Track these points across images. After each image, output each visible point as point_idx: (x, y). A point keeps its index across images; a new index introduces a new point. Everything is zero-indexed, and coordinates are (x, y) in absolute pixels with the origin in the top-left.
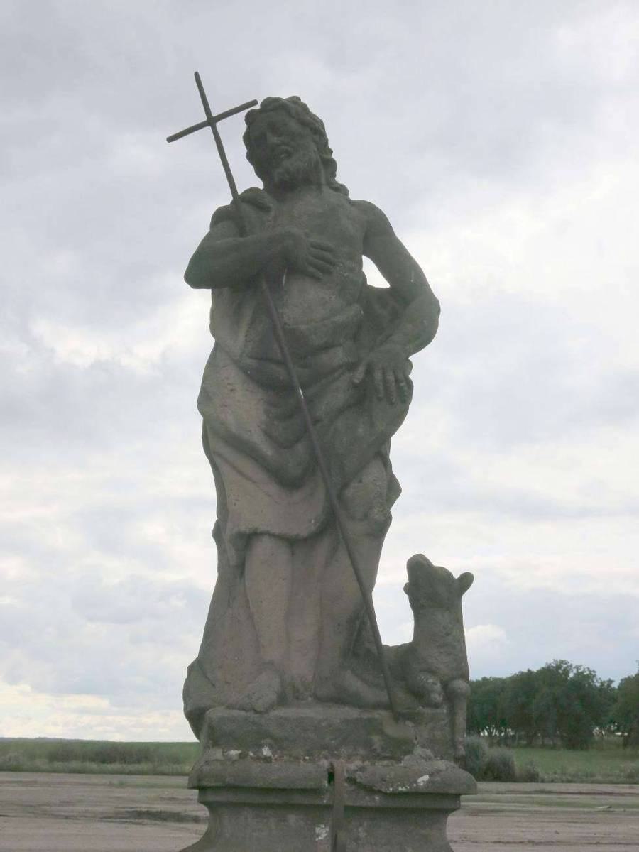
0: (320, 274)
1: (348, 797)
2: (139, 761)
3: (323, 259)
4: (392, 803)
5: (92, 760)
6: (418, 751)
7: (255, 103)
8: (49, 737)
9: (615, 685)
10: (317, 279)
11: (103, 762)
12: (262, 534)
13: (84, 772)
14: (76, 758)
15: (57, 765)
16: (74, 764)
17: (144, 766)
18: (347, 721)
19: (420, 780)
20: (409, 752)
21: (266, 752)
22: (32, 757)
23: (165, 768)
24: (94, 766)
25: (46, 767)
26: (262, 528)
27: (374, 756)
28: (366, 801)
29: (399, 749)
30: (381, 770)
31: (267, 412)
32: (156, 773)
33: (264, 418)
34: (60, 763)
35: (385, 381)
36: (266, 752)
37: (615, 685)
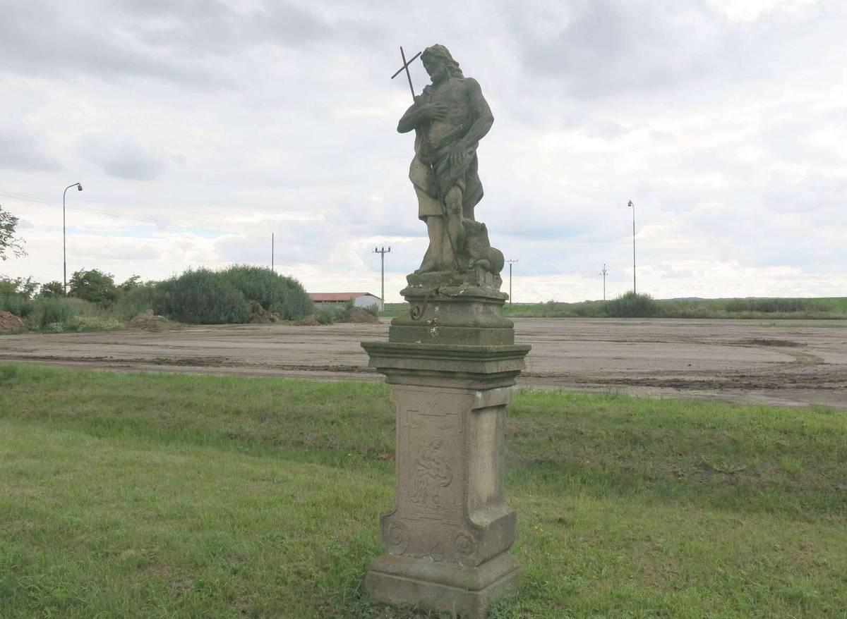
0: (441, 119)
1: (441, 298)
2: (794, 310)
3: (442, 113)
4: (455, 299)
5: (758, 310)
6: (465, 283)
7: (421, 53)
8: (755, 297)
9: (102, 276)
10: (441, 121)
11: (767, 311)
12: (429, 216)
13: (753, 318)
14: (746, 309)
15: (734, 314)
16: (745, 313)
17: (797, 313)
18: (442, 275)
19: (461, 292)
20: (462, 284)
21: (421, 285)
22: (715, 309)
23: (814, 315)
24: (760, 314)
25: (724, 315)
26: (427, 214)
27: (450, 285)
28: (447, 299)
29: (458, 283)
30: (451, 289)
31: (427, 174)
32: (807, 318)
33: (426, 175)
34: (735, 313)
35: (453, 159)
36: (421, 285)
37: (102, 276)
